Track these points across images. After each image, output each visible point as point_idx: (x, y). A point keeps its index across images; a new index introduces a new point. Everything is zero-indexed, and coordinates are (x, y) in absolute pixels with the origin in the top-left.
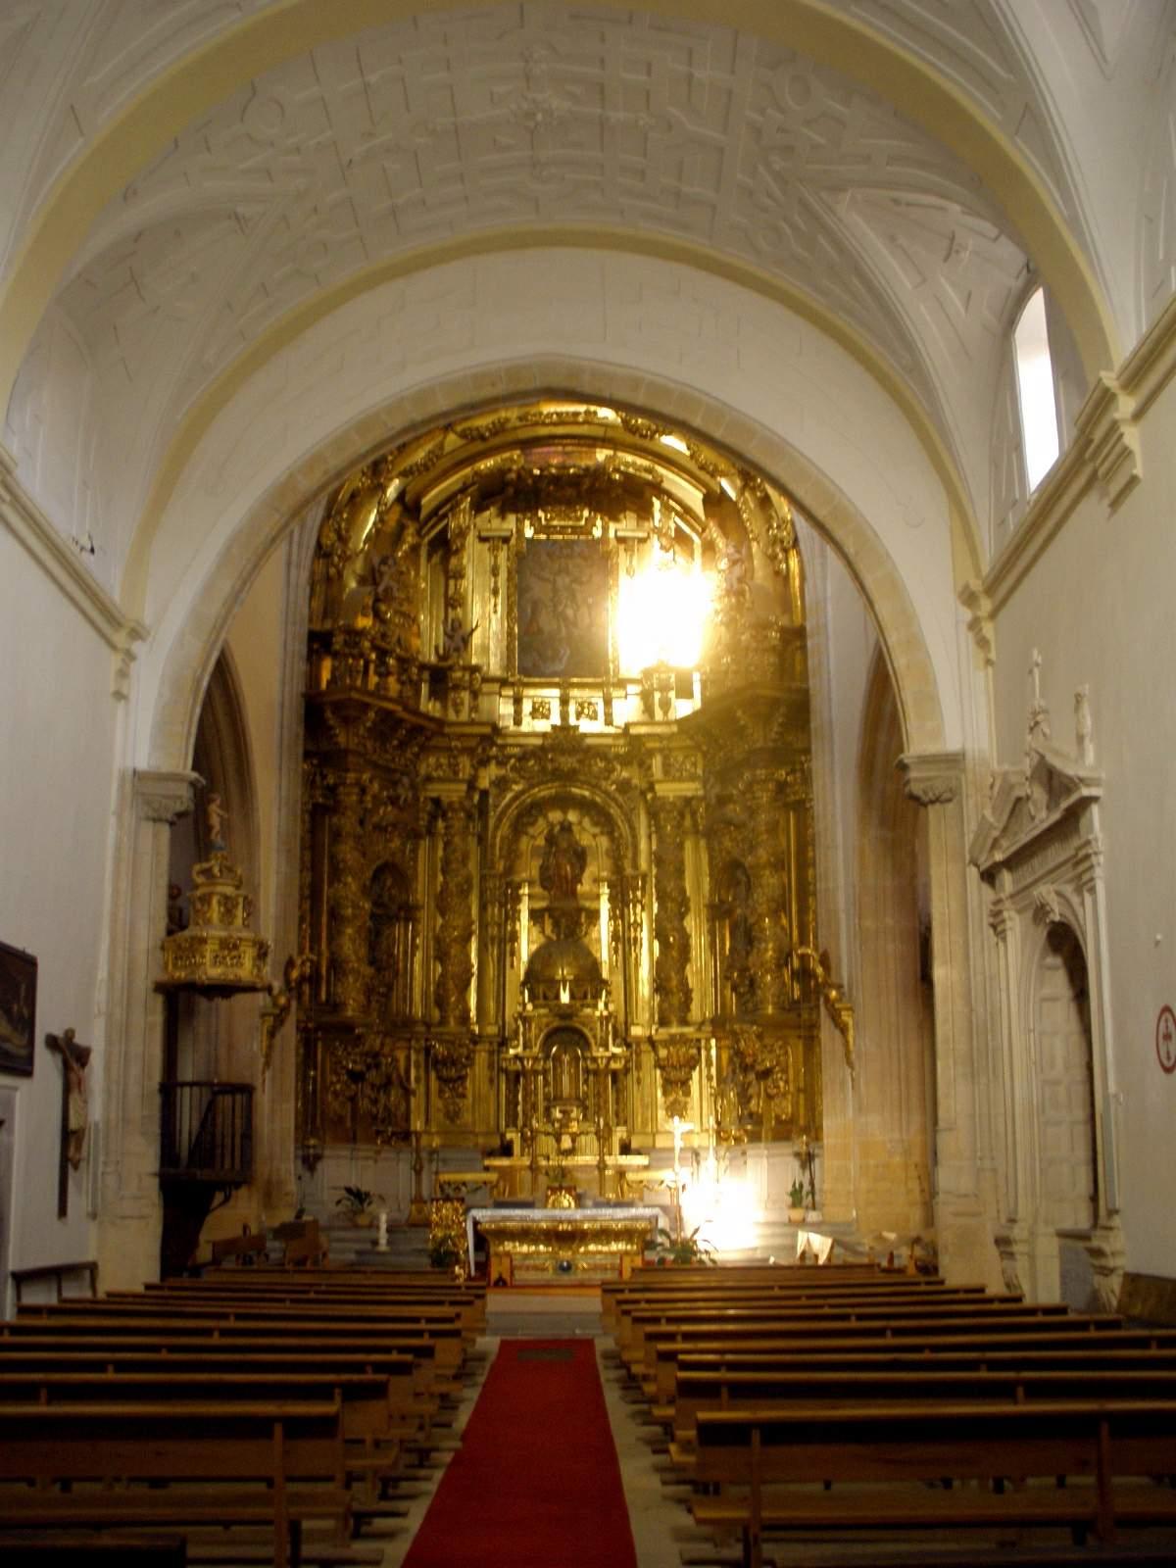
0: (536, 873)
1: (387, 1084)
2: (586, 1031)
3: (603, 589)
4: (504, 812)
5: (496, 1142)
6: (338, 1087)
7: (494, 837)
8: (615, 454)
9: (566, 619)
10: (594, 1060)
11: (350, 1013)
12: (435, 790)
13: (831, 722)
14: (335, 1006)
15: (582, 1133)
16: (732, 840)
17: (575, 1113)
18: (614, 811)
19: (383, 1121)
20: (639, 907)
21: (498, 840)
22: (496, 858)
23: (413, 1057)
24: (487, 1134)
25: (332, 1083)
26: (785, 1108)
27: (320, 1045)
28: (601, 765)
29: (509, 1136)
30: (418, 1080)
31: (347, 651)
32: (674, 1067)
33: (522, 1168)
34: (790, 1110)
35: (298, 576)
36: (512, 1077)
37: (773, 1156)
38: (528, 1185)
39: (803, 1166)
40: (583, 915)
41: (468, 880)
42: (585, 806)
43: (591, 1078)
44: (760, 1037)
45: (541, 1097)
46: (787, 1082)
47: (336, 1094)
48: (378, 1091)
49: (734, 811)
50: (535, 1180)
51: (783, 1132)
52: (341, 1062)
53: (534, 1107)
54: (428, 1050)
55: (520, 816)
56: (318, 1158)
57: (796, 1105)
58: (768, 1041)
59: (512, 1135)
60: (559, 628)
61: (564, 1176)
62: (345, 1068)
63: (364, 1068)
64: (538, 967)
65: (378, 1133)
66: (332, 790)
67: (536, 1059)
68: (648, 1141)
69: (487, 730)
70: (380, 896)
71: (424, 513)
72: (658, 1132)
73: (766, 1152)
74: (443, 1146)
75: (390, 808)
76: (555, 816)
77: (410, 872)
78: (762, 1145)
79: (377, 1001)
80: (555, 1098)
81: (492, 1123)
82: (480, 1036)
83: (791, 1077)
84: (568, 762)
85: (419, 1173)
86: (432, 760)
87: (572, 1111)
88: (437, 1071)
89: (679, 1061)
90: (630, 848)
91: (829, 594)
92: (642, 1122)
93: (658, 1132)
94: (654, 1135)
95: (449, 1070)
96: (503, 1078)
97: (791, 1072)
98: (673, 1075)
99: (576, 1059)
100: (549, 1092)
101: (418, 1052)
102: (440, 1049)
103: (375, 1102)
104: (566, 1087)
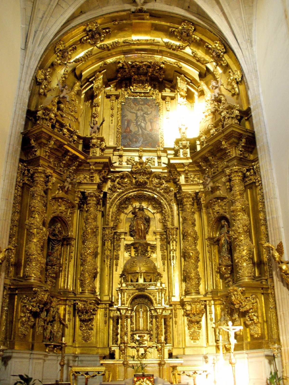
0: (127, 230)
1: (52, 322)
2: (151, 297)
3: (157, 116)
4: (113, 201)
5: (107, 352)
6: (24, 319)
7: (109, 211)
8: (162, 57)
9: (141, 127)
10: (155, 310)
11: (32, 281)
12: (82, 188)
13: (267, 142)
14: (26, 277)
16: (219, 206)
17: (146, 337)
18: (163, 202)
19: (50, 339)
20: (175, 242)
21: (111, 213)
22: (110, 221)
23: (68, 308)
24: (104, 348)
25: (21, 317)
26: (257, 330)
27: (16, 297)
28: (157, 181)
29: (113, 349)
30: (69, 320)
31: (43, 117)
32: (194, 314)
33: (119, 365)
34: (260, 332)
35: (24, 85)
36: (115, 320)
37: (251, 357)
38: (122, 374)
39: (270, 363)
40: (149, 247)
41: (97, 227)
42: (150, 200)
43: (154, 320)
44: (243, 293)
45: (129, 330)
46: (258, 317)
47: (23, 324)
48: (48, 324)
49: (220, 193)
50: (126, 371)
51: (257, 343)
52: (26, 306)
53: (126, 334)
54: (74, 305)
55: (121, 204)
56: (9, 358)
57: (263, 329)
58: (247, 295)
59: (115, 349)
60: (139, 130)
62: (28, 309)
63: (38, 310)
64: (128, 267)
65: (47, 345)
66: (32, 177)
67: (127, 310)
68: (180, 352)
69: (107, 160)
70: (54, 230)
71: (83, 78)
74: (81, 353)
75: (61, 192)
76: (137, 204)
77: (69, 222)
78: (244, 352)
79: (51, 281)
80: (136, 330)
83: (260, 315)
84: (142, 179)
86: (82, 176)
87: (145, 336)
88: (79, 316)
89: (196, 311)
90: (170, 217)
91: (261, 91)
94: (184, 348)
95: (85, 316)
96: (111, 321)
97: (259, 311)
98: (194, 319)
99: (147, 311)
101: (70, 306)
102: (80, 305)
103: (45, 329)
104: (141, 325)
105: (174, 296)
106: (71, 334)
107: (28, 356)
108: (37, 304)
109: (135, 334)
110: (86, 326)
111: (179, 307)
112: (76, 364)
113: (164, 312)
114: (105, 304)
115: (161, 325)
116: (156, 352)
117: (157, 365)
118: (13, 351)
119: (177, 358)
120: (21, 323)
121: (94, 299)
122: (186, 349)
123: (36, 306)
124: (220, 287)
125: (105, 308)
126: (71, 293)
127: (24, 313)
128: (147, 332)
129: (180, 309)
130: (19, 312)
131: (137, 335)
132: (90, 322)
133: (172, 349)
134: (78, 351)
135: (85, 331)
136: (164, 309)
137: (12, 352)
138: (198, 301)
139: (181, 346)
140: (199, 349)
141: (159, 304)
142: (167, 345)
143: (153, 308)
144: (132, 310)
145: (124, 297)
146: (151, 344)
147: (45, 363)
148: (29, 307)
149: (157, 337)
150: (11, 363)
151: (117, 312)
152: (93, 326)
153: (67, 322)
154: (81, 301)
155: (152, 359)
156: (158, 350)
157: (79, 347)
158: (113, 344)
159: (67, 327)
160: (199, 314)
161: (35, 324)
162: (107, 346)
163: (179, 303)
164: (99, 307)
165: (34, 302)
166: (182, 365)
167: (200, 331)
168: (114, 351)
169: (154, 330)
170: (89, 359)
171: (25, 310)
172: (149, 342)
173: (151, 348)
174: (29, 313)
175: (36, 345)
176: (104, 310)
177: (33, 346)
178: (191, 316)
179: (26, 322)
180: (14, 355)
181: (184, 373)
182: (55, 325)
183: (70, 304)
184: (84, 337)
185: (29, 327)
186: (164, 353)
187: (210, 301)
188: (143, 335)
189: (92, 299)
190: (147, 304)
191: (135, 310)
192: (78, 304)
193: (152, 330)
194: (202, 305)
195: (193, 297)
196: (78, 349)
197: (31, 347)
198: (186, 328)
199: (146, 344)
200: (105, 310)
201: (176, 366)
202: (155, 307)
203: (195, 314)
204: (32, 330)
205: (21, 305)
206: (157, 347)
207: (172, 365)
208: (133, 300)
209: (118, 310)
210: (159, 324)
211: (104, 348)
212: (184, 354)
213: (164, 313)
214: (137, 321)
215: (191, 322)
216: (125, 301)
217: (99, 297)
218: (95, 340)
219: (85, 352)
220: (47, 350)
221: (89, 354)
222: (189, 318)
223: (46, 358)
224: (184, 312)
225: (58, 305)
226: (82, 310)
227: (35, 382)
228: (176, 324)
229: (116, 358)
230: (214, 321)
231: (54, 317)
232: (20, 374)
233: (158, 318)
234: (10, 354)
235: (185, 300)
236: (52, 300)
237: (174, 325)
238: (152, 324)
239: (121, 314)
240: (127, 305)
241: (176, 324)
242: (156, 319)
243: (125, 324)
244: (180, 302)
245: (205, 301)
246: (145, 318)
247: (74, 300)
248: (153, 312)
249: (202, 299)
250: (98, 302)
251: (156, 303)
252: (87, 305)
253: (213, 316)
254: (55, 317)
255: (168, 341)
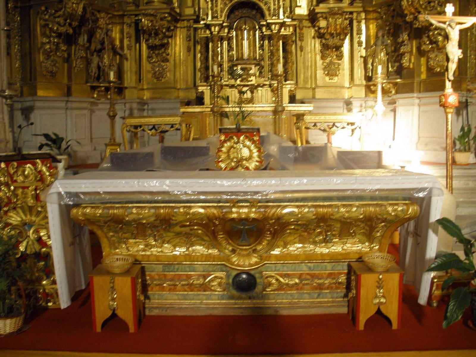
2: (262, 5)
5: (193, 96)
10: (269, 26)
15: (259, 86)
17: (254, 70)
23: (126, 29)
24: (187, 89)
25: (43, 44)
29: (201, 89)
32: (332, 35)
37: (425, 104)
47: (48, 55)
54: (137, 23)
59: (204, 89)
61: (244, 118)
62: (51, 30)
65: (93, 88)
67: (221, 27)
72: (317, 86)
73: (417, 101)
74: (152, 98)
80: (237, 60)
81: (189, 81)
82: (180, 15)
85: (112, 118)
87: (251, 69)
92: (304, 80)
93: (317, 86)
94: (314, 89)
98: (331, 42)
100: (233, 55)
102: (145, 22)
103: (88, 63)
105: (300, 6)
106: (134, 69)
107: (63, 104)
108: (66, 20)
109: (236, 65)
110: (157, 55)
111: (306, 23)
112: (145, 113)
113: (283, 30)
114: (188, 20)
115: (278, 50)
116: (270, 93)
117: (271, 113)
118: (35, 98)
119: (302, 102)
120: (43, 53)
121: (168, 11)
122: (317, 90)
123: (65, 24)
124: (369, 73)
125: (187, 27)
126: (131, 5)
127: (49, 37)
128: (255, 62)
129: (309, 27)
130: (39, 35)
131: (239, 67)
132: (163, 50)
133: (295, 88)
134: (147, 95)
135: (157, 64)
136: (283, 25)
137: (34, 101)
138: (340, 12)
139: (309, 86)
140: (338, 90)
141: (274, 15)
142: (288, 82)
143: (265, 23)
144: (230, 28)
145: (217, 6)
146: (261, 81)
147: (94, 114)
148: (53, 25)
149: (271, 71)
150: (35, 116)
151: (205, 32)
152: (168, 55)
153: (126, 51)
154: (146, 15)
155: (262, 104)
156: (272, 91)
157: (147, 89)
158: (201, 82)
159: (127, 59)
160: (339, 34)
161: (69, 55)
162: (192, 86)
163: (307, 18)
164: (178, 25)
165: (59, 17)
166: (310, 113)
167: (340, 62)
168: (202, 93)
169: (267, 59)
170: (165, 106)
171: (48, 32)
172: (258, 79)
173: (262, 87)
174: (56, 37)
175: (74, 87)
176: (186, 29)
177: (69, 89)
178: (327, 36)
179: (51, 52)
180: (38, 104)
181: (315, 125)
182: (105, 56)
183: (129, 22)
184: (155, 73)
185: (60, 60)
186: (282, 94)
187: (359, 13)
188: (248, 66)
189: (163, 11)
190: (254, 18)
191: (236, 27)
192: (141, 20)
193: (263, 59)
194: (346, 19)
195: (332, 6)
196: (146, 92)
197: (66, 91)
198: (318, 57)
199: (253, 80)
200: (188, 30)
201: (303, 115)
202: (268, 21)
203: (333, 34)
204: (66, 65)
205: (40, 25)
206: (270, 86)
207: (295, 113)
208: (232, 10)
209: (208, 27)
210: (275, 48)
211: (187, 89)
212: (314, 97)
213: (283, 32)
214: (240, 46)
215: (325, 47)
216: (219, 12)
217: (178, 10)
218: (172, 77)
219: (157, 96)
220: (95, 96)
221: (164, 99)
222: (324, 41)
223: (95, 108)
224: (316, 31)
225: (109, 24)
226: (149, 30)
227: (69, 144)
228: (301, 51)
229: (206, 103)
230: (364, 45)
231: (102, 43)
232: (46, 132)
233: (273, 39)
234: (31, 103)
235: (317, 11)
236: (98, 16)
237: (299, 52)
238: (263, 50)
239: (211, 33)
240: (223, 19)
241: (301, 51)
242: (269, 42)
243: (219, 49)
244: (309, 15)
245: (351, 13)
246: (252, 40)
247: (136, 15)
248: (264, 29)
249: (346, 10)
250: (176, 18)
251: (270, 14)
252: (157, 22)
253: (363, 38)
254: (104, 42)
255: (290, 77)
